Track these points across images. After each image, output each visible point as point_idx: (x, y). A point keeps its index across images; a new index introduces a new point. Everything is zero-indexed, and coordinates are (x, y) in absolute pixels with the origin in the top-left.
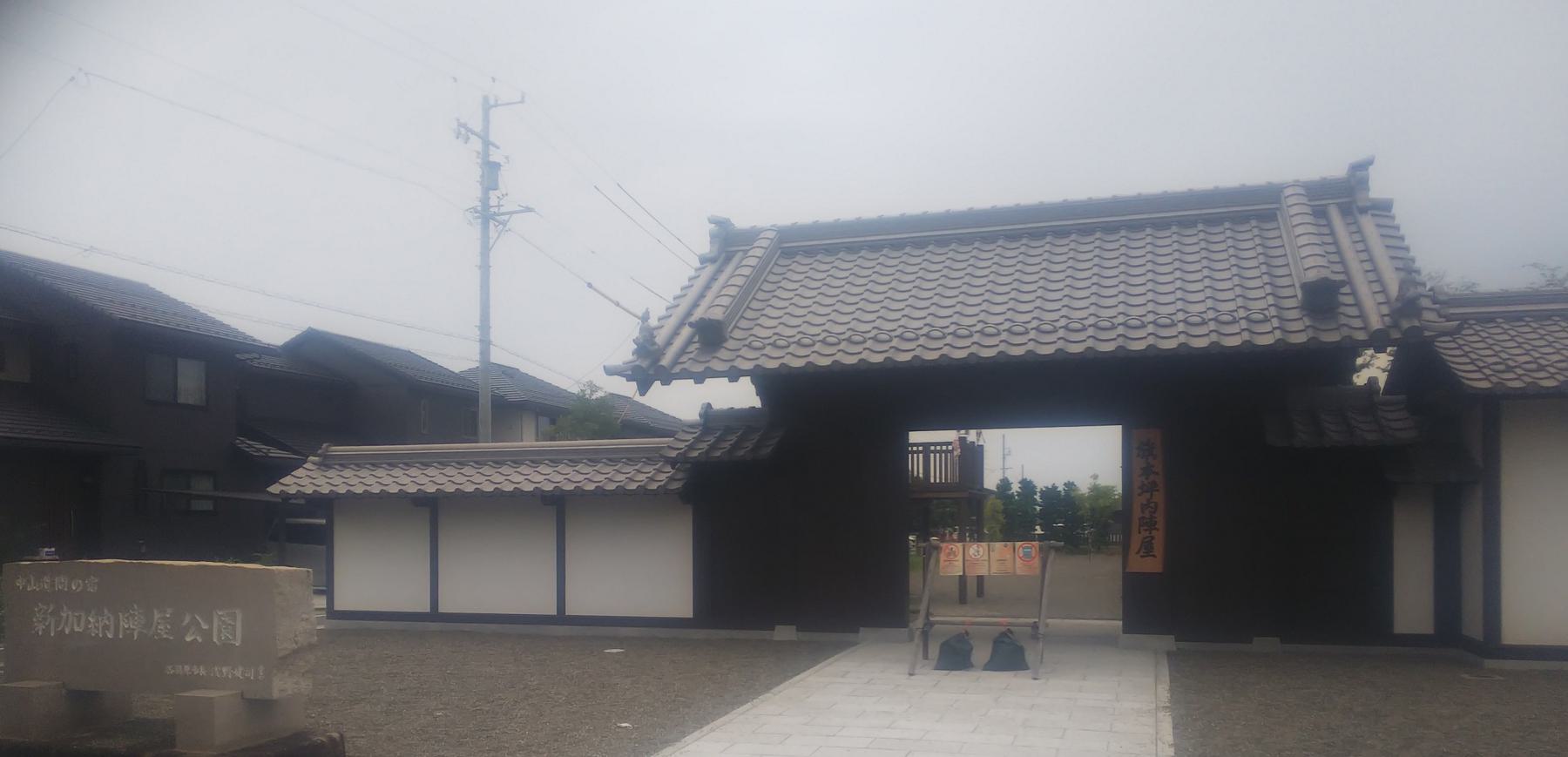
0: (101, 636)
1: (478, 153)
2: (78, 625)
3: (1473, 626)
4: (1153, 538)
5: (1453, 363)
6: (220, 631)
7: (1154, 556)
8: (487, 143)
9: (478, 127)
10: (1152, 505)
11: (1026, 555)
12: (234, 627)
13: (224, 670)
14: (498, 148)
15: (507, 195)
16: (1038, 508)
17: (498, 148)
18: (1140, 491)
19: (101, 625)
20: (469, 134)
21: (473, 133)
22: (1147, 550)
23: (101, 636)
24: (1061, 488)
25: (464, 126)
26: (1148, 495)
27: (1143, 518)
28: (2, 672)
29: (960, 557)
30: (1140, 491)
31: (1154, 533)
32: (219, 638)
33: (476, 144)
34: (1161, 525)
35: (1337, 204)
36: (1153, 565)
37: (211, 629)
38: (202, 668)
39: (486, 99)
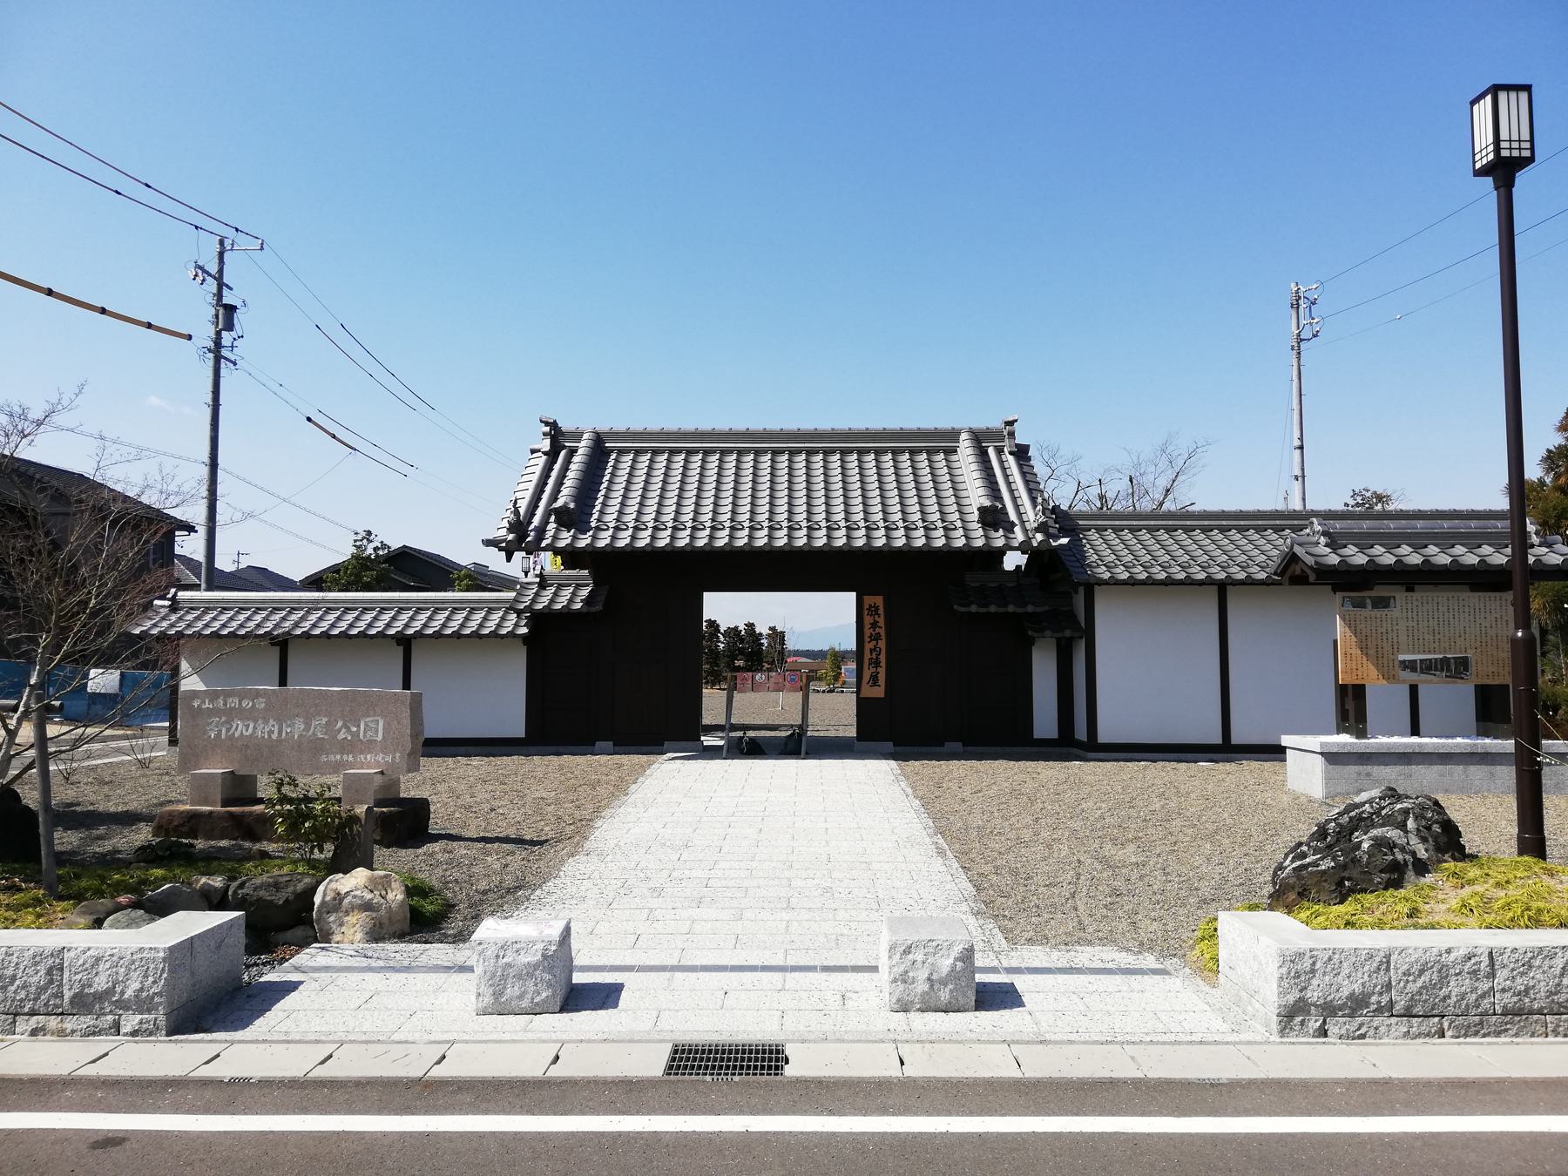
0: (266, 737)
1: (214, 295)
2: (247, 731)
3: (1081, 733)
4: (878, 673)
5: (1065, 555)
6: (365, 732)
7: (879, 686)
8: (221, 285)
9: (214, 269)
10: (878, 649)
11: (792, 680)
12: (377, 731)
13: (369, 756)
14: (231, 289)
15: (242, 337)
16: (722, 646)
17: (231, 289)
18: (869, 639)
19: (267, 730)
20: (206, 275)
21: (210, 275)
22: (874, 680)
23: (266, 737)
24: (742, 627)
25: (201, 268)
26: (875, 642)
27: (872, 658)
28: (1566, 606)
29: (750, 682)
30: (869, 639)
31: (879, 669)
32: (365, 736)
33: (212, 285)
34: (883, 664)
35: (995, 446)
36: (879, 692)
37: (359, 731)
38: (351, 756)
39: (1460, 853)
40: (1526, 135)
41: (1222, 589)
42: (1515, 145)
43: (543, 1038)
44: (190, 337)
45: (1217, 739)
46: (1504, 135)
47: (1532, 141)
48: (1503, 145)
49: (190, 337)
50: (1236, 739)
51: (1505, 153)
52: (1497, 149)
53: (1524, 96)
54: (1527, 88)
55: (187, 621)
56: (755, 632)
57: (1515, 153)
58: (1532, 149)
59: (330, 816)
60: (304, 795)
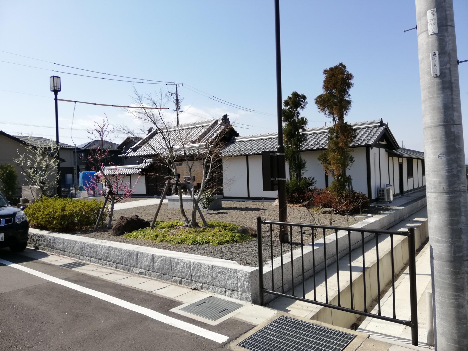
40: (59, 86)
41: (247, 156)
42: (57, 88)
43: (432, 27)
44: (168, 108)
45: (247, 196)
46: (55, 85)
47: (60, 87)
48: (55, 87)
49: (168, 108)
50: (250, 196)
51: (55, 89)
52: (54, 88)
53: (59, 78)
54: (60, 77)
55: (140, 160)
56: (347, 125)
57: (58, 89)
58: (60, 89)
59: (206, 203)
60: (328, 138)
